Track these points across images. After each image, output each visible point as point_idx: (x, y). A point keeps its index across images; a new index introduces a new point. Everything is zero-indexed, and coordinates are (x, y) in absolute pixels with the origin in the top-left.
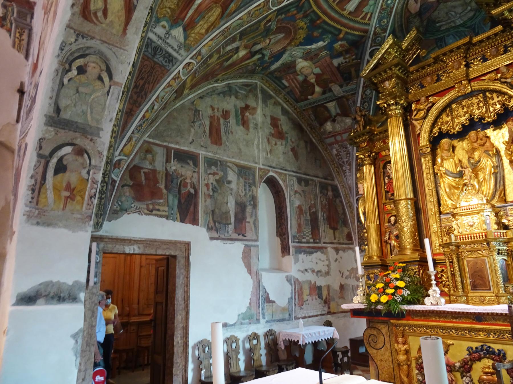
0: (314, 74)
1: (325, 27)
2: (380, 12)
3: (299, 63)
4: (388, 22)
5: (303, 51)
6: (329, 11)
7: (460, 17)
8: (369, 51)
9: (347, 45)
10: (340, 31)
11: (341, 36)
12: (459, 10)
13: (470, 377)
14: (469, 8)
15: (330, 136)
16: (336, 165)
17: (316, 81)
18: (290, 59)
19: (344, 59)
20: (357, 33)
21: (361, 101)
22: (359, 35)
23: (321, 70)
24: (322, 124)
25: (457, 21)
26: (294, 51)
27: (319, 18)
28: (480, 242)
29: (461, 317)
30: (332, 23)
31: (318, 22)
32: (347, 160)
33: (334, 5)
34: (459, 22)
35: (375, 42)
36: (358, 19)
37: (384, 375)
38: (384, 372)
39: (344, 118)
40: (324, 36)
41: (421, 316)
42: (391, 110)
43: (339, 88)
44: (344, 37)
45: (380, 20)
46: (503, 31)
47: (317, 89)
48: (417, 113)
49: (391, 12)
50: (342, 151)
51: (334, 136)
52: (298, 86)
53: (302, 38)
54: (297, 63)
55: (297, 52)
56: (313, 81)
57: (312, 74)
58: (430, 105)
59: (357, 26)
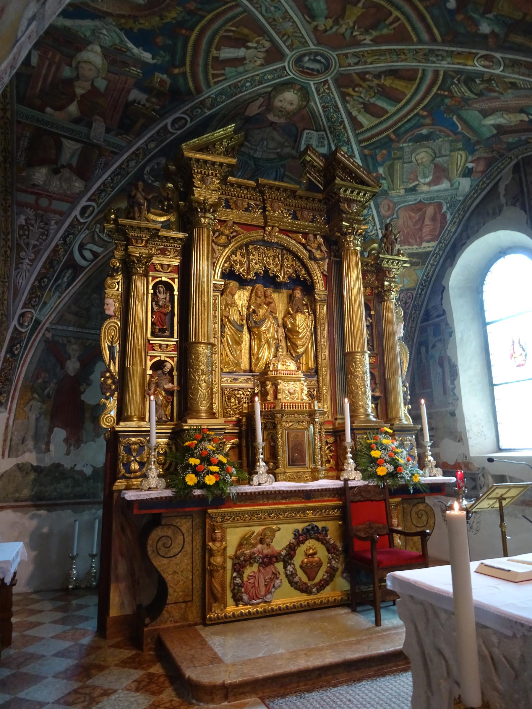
0: (92, 84)
1: (180, 45)
2: (230, 86)
3: (92, 51)
4: (223, 102)
5: (117, 41)
6: (209, 33)
7: (264, 151)
8: (178, 115)
9: (168, 87)
10: (183, 64)
11: (176, 71)
12: (272, 145)
13: (293, 564)
14: (279, 150)
15: (30, 190)
16: (9, 243)
17: (83, 96)
18: (88, 34)
19: (147, 100)
20: (191, 84)
21: (116, 170)
22: (190, 89)
23: (107, 87)
24: (33, 163)
25: (258, 153)
26: (108, 30)
27: (192, 29)
28: (302, 413)
29: (292, 496)
30: (190, 49)
31: (184, 31)
32: (36, 243)
33: (222, 33)
34: (258, 155)
35: (192, 112)
36: (211, 71)
37: (176, 594)
38: (177, 590)
39: (74, 177)
40: (162, 52)
41: (246, 500)
42: (205, 218)
43: (103, 130)
44: (176, 75)
45: (221, 93)
46: (320, 201)
47: (73, 109)
48: (219, 236)
49: (236, 95)
50: (36, 227)
51: (39, 195)
52: (50, 79)
53: (141, 26)
54: (89, 48)
55: (110, 35)
56: (79, 91)
57: (90, 82)
58: (235, 234)
59: (201, 77)
